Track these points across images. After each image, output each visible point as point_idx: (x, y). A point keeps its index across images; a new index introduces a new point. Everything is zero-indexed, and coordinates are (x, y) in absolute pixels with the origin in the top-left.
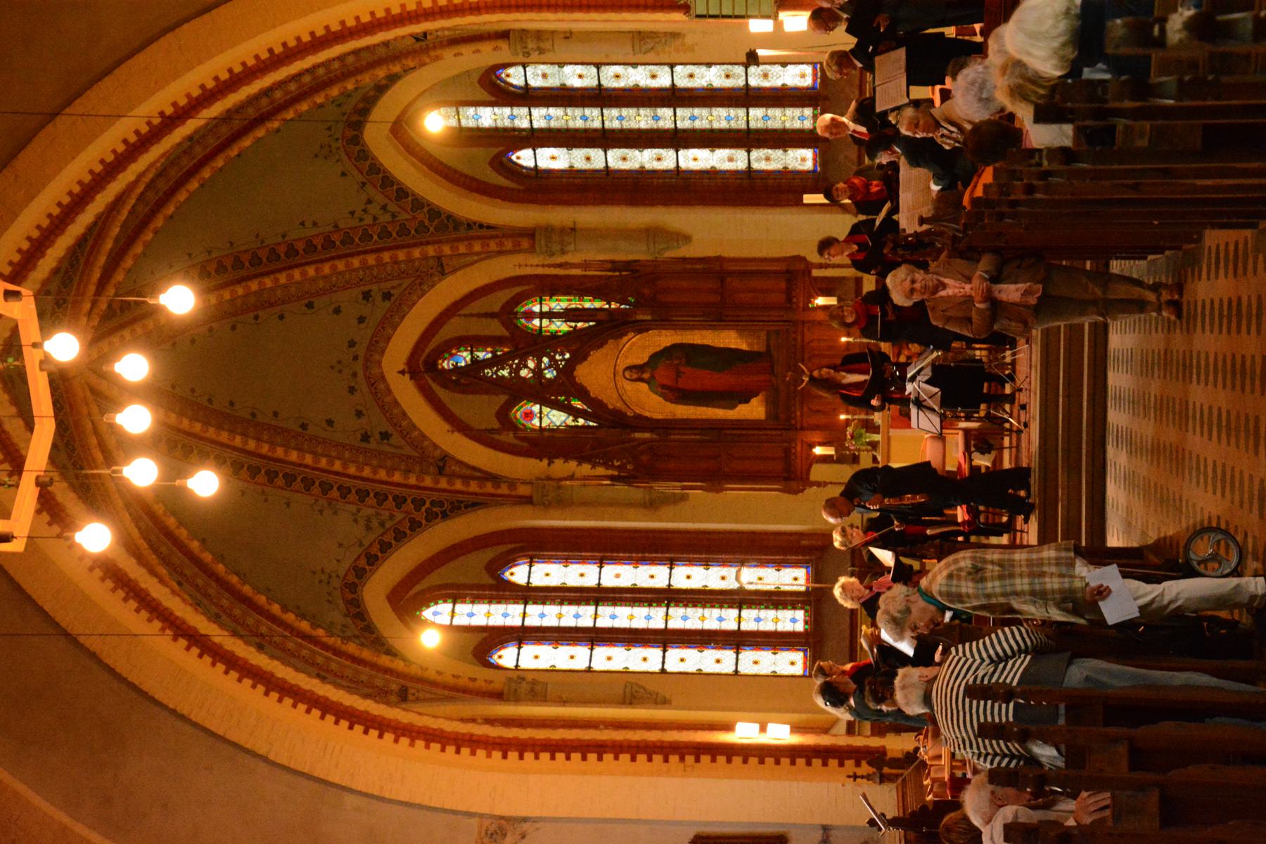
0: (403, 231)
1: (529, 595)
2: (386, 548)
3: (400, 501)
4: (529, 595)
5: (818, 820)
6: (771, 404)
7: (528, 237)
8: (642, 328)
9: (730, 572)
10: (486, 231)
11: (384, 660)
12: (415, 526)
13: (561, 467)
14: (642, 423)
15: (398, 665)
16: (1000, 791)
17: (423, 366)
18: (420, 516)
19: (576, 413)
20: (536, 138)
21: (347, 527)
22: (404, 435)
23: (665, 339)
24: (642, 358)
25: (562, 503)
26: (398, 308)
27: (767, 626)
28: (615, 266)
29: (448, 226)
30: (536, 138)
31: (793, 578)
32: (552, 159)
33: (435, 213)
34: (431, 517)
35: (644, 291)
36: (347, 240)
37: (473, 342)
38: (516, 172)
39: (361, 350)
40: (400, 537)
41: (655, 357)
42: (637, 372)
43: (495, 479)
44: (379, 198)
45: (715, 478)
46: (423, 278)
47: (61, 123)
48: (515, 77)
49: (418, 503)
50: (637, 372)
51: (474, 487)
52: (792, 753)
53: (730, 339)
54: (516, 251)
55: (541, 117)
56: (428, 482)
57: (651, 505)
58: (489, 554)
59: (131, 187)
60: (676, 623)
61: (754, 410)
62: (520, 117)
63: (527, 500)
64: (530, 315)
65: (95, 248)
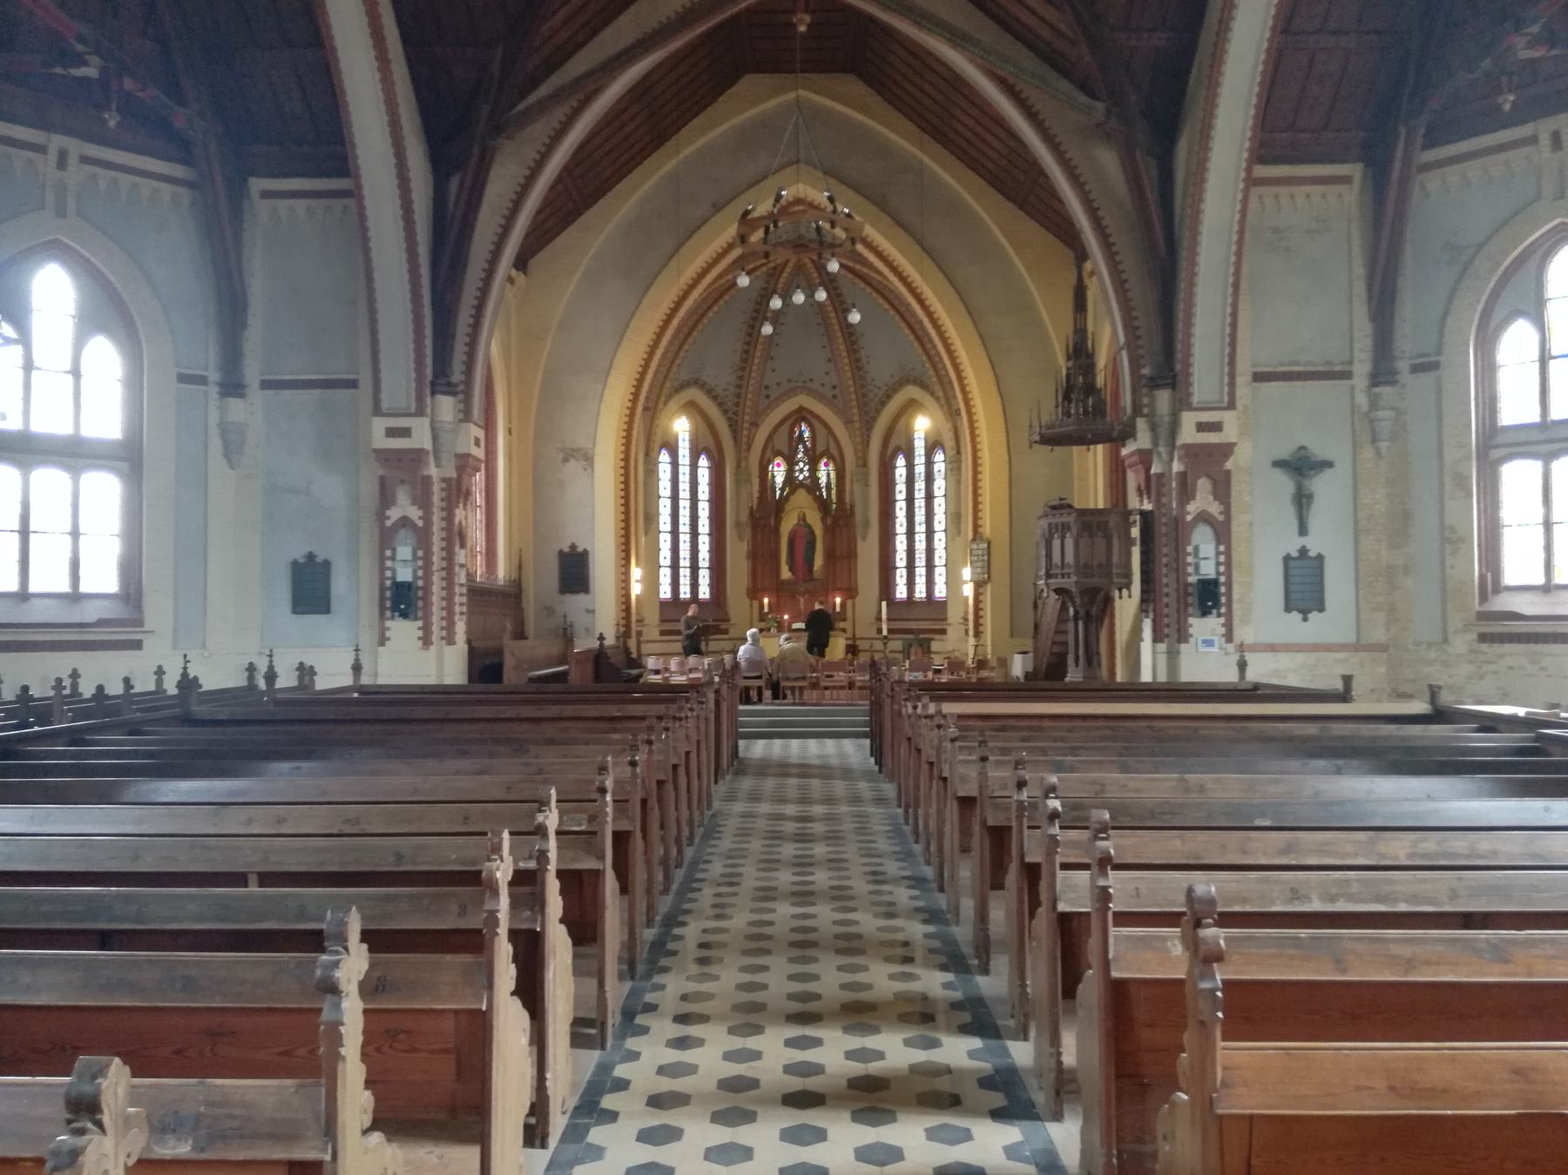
0: (866, 404)
1: (694, 467)
2: (715, 398)
3: (737, 405)
4: (694, 467)
5: (597, 607)
6: (788, 582)
7: (863, 463)
8: (823, 520)
9: (707, 564)
10: (866, 444)
11: (663, 399)
12: (725, 412)
13: (756, 481)
14: (778, 520)
15: (660, 406)
16: (538, 1142)
17: (801, 415)
18: (730, 415)
19: (782, 489)
20: (910, 467)
21: (724, 379)
22: (768, 407)
23: (818, 531)
24: (809, 521)
25: (738, 482)
26: (830, 402)
27: (682, 580)
28: (852, 507)
29: (868, 425)
30: (910, 467)
31: (704, 592)
32: (900, 472)
33: (874, 419)
34: (729, 419)
35: (839, 518)
36: (864, 396)
37: (813, 437)
38: (894, 457)
39: (809, 384)
40: (720, 405)
41: (810, 527)
42: (803, 518)
43: (749, 449)
44: (880, 393)
45: (753, 555)
46: (843, 413)
47: (917, 248)
48: (939, 457)
49: (736, 413)
50: (803, 518)
51: (745, 439)
52: (627, 595)
53: (819, 561)
54: (857, 458)
55: (920, 469)
56: (747, 418)
57: (738, 525)
58: (713, 448)
59: (881, 274)
60: (682, 537)
61: (786, 574)
62: (920, 460)
63: (738, 465)
64: (826, 465)
65: (855, 261)
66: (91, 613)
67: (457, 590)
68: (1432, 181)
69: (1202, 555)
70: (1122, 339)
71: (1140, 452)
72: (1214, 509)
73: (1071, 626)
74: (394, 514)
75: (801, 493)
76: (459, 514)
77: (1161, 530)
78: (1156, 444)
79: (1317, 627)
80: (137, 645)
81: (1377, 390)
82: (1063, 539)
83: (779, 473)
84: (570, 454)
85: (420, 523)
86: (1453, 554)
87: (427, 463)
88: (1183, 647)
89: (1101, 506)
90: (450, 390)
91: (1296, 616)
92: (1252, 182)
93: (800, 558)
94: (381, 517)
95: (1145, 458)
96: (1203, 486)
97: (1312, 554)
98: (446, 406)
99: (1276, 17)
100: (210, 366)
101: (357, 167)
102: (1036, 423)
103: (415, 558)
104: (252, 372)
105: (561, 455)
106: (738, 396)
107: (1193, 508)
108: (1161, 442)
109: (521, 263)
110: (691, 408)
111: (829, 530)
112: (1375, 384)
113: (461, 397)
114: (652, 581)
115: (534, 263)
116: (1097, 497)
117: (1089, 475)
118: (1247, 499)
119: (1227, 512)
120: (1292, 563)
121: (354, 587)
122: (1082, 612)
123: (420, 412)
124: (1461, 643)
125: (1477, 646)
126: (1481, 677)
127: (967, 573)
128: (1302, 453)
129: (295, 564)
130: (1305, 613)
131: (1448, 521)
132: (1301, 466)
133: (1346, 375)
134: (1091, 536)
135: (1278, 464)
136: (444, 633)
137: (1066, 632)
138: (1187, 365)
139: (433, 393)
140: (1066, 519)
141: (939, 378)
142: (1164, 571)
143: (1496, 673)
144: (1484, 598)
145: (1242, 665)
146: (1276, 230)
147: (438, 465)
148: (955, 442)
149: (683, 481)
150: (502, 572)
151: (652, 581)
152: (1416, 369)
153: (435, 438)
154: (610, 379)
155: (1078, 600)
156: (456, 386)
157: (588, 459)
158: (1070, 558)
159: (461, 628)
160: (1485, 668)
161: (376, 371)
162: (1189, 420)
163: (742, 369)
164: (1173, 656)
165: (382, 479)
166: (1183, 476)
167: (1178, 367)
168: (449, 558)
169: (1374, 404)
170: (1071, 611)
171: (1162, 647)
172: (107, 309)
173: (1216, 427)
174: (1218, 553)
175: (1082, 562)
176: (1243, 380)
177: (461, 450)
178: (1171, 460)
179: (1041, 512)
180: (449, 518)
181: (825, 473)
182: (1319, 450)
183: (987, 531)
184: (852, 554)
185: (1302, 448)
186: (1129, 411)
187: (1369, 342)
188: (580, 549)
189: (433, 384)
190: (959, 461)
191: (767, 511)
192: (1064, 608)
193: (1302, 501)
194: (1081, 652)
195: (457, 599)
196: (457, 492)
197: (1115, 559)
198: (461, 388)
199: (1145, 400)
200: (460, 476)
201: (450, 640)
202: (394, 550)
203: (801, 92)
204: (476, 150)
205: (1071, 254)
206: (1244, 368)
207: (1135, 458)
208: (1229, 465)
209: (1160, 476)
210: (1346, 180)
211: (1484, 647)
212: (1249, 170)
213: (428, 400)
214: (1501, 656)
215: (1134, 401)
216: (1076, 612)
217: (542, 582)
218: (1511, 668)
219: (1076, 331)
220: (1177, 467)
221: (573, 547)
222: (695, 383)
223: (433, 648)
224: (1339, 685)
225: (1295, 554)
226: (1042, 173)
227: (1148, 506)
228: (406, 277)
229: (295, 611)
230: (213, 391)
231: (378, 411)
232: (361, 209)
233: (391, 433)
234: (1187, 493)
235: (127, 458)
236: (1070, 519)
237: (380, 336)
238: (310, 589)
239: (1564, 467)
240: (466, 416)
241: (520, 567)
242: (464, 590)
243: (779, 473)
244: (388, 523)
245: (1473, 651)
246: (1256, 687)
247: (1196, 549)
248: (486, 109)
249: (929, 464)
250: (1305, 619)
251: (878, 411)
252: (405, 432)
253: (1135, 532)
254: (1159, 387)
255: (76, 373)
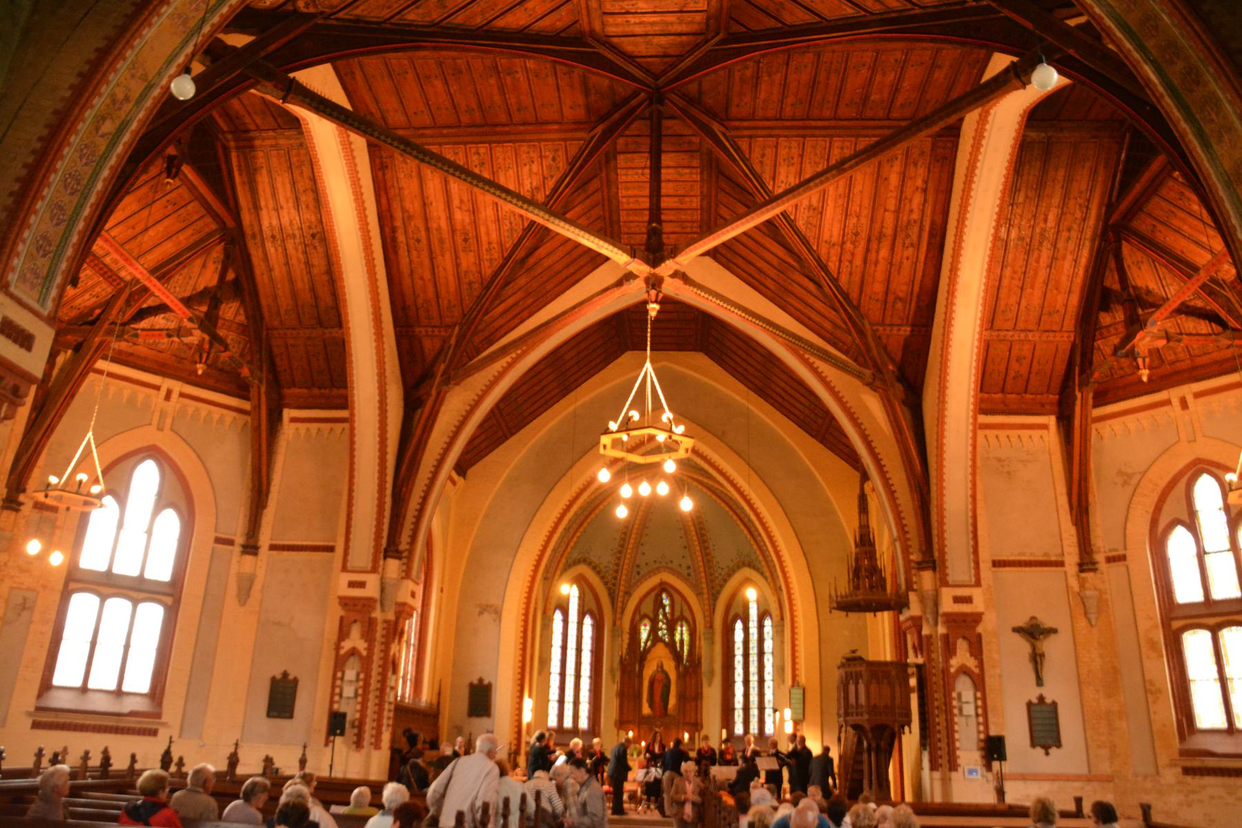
0: (712, 581)
3: (615, 578)
6: (648, 717)
8: (677, 668)
11: (558, 572)
12: (606, 584)
13: (626, 637)
14: (642, 667)
17: (663, 587)
20: (746, 630)
24: (666, 668)
25: (613, 637)
26: (686, 578)
29: (715, 596)
30: (746, 630)
31: (584, 724)
33: (719, 593)
34: (609, 589)
35: (691, 669)
36: (711, 574)
37: (672, 606)
38: (734, 622)
40: (602, 578)
45: (622, 695)
48: (768, 623)
52: (519, 721)
53: (672, 701)
54: (705, 622)
55: (753, 630)
56: (622, 588)
57: (612, 670)
58: (595, 609)
59: (718, 482)
61: (646, 710)
63: (614, 624)
66: (128, 705)
67: (386, 706)
68: (1106, 428)
69: (964, 699)
70: (895, 533)
71: (912, 618)
72: (971, 663)
73: (865, 756)
74: (347, 645)
75: (660, 646)
76: (394, 648)
77: (936, 680)
78: (925, 613)
79: (1057, 761)
80: (154, 733)
81: (1083, 575)
82: (857, 684)
83: (644, 633)
84: (484, 609)
85: (364, 653)
86: (1154, 702)
87: (374, 609)
88: (954, 775)
89: (889, 658)
90: (398, 555)
91: (1039, 751)
92: (977, 427)
93: (657, 698)
94: (338, 647)
95: (917, 623)
96: (962, 646)
97: (1048, 700)
98: (393, 567)
99: (982, 319)
100: (237, 529)
101: (353, 402)
102: (833, 593)
103: (358, 679)
104: (265, 540)
105: (478, 610)
106: (616, 571)
107: (955, 662)
108: (928, 610)
109: (462, 468)
110: (580, 581)
111: (681, 677)
112: (1082, 571)
113: (405, 561)
114: (541, 711)
115: (471, 472)
116: (883, 651)
117: (878, 637)
118: (996, 656)
119: (981, 665)
120: (1033, 708)
121: (311, 705)
122: (874, 745)
123: (374, 570)
124: (1171, 776)
125: (1182, 777)
126: (1189, 805)
127: (788, 713)
128: (1034, 622)
129: (273, 679)
130: (1046, 748)
131: (1147, 677)
132: (1033, 632)
133: (1061, 564)
134: (878, 683)
135: (1017, 630)
136: (373, 740)
137: (861, 762)
138: (943, 553)
139: (385, 558)
140: (858, 669)
141: (767, 562)
142: (936, 712)
143: (1201, 801)
144: (1182, 738)
145: (1000, 792)
146: (999, 460)
147: (383, 611)
148: (778, 610)
149: (571, 638)
150: (425, 697)
151: (541, 711)
152: (1110, 560)
153: (383, 590)
154: (519, 555)
155: (870, 735)
156: (402, 552)
157: (498, 613)
158: (862, 700)
159: (386, 737)
160: (1192, 797)
161: (347, 540)
162: (947, 594)
163: (620, 552)
164: (946, 782)
165: (342, 618)
166: (946, 638)
167: (936, 554)
168: (383, 681)
169: (1082, 585)
170: (865, 743)
171: (937, 775)
172: (179, 493)
173: (968, 600)
174: (976, 699)
175: (872, 703)
176: (985, 566)
177: (401, 599)
178: (936, 624)
179: (839, 662)
180: (386, 651)
181: (682, 633)
182: (1047, 622)
183: (802, 679)
184: (698, 697)
185: (1033, 618)
186: (903, 587)
187: (1074, 539)
188: (486, 682)
189: (386, 550)
190: (783, 626)
191: (635, 658)
192: (860, 743)
193: (1037, 659)
194: (874, 777)
195: (386, 713)
196: (395, 631)
197: (898, 701)
198: (405, 554)
199: (914, 579)
200: (397, 618)
201: (377, 746)
202: (343, 673)
203: (665, 363)
204: (434, 392)
205: (857, 475)
206: (985, 557)
207: (910, 623)
208: (980, 629)
209: (929, 637)
210: (1045, 427)
211: (1189, 779)
212: (975, 419)
213: (381, 562)
214: (1204, 787)
215: (906, 580)
216: (869, 745)
217: (454, 708)
218: (1212, 797)
219: (861, 527)
220: (941, 630)
221: (481, 680)
222: (584, 561)
223: (364, 751)
224: (1072, 807)
225: (1035, 701)
226: (833, 418)
227: (920, 660)
228: (377, 475)
229: (269, 715)
230: (237, 549)
231: (344, 569)
232: (352, 429)
233: (352, 584)
234: (950, 650)
235: (170, 594)
236: (863, 669)
237: (285, 553)
238: (281, 698)
239: (1230, 636)
240: (407, 574)
241: (439, 694)
242: (392, 707)
243: (644, 633)
244: (342, 652)
245: (1180, 782)
246: (1010, 807)
247: (959, 695)
248: (443, 367)
249: (761, 627)
250: (1047, 754)
251: (722, 586)
252: (362, 585)
253: (913, 682)
254: (923, 569)
255: (149, 532)
